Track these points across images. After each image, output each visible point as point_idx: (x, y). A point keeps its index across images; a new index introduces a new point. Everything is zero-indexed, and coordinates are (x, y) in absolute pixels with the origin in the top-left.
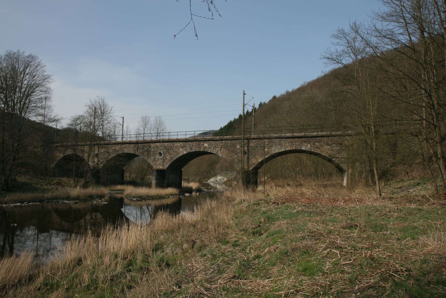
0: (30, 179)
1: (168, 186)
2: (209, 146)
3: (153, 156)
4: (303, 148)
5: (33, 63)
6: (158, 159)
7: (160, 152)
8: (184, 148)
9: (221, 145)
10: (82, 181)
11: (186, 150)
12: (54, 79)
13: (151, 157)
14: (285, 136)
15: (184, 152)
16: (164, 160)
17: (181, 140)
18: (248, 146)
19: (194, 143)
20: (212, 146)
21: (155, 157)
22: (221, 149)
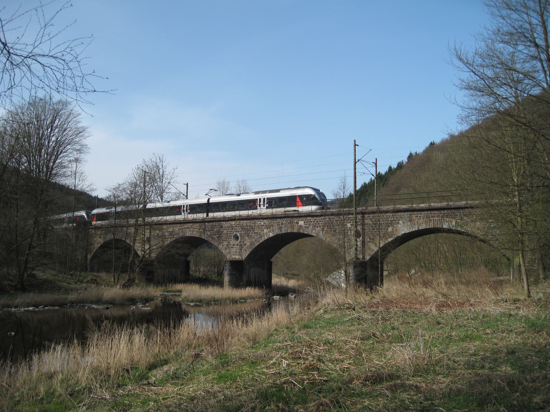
0: (55, 275)
1: (249, 284)
2: (306, 224)
3: (226, 241)
4: (445, 226)
5: (63, 111)
6: (234, 245)
7: (236, 234)
8: (270, 228)
9: (324, 223)
10: (126, 276)
11: (273, 230)
12: (91, 132)
13: (223, 242)
14: (417, 208)
15: (270, 234)
16: (241, 247)
17: (265, 217)
18: (363, 224)
19: (284, 221)
20: (310, 225)
21: (229, 242)
22: (323, 229)
